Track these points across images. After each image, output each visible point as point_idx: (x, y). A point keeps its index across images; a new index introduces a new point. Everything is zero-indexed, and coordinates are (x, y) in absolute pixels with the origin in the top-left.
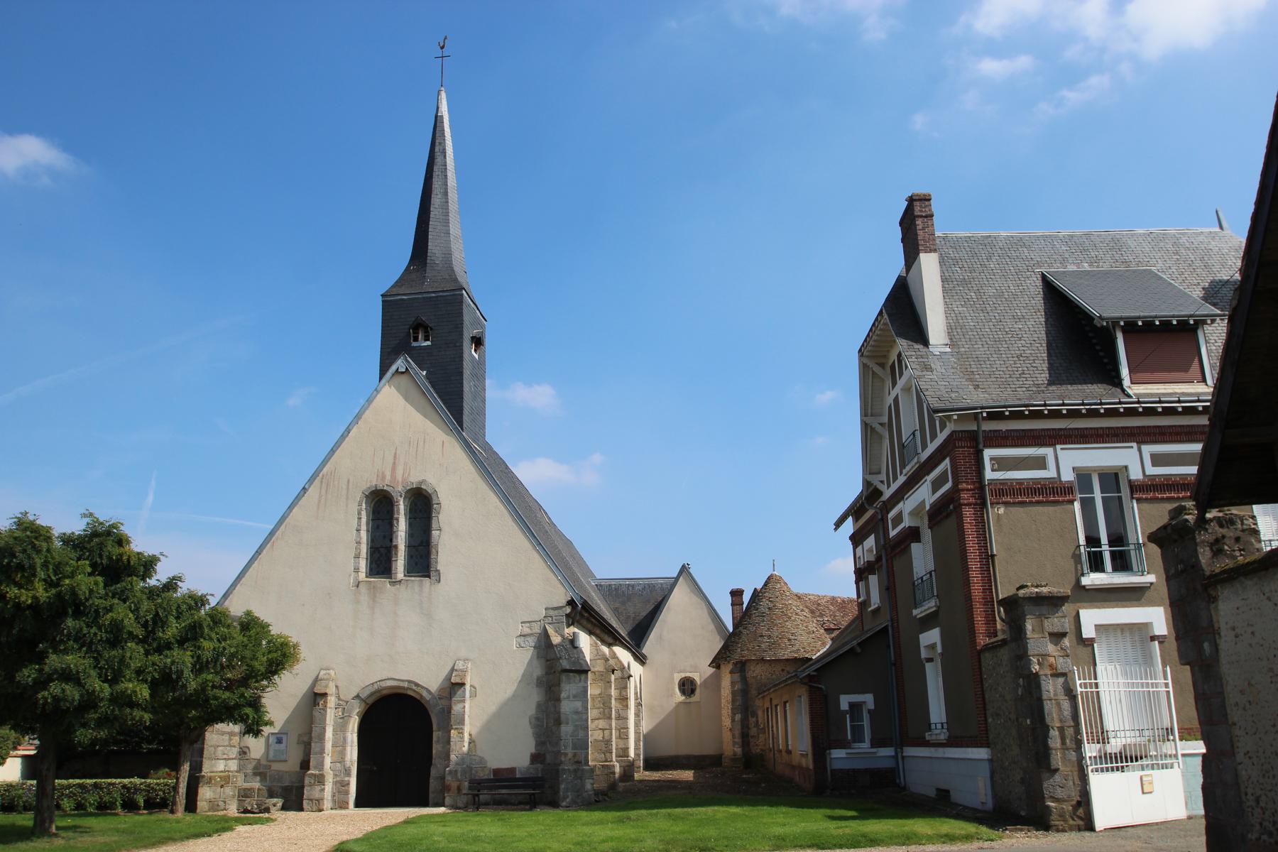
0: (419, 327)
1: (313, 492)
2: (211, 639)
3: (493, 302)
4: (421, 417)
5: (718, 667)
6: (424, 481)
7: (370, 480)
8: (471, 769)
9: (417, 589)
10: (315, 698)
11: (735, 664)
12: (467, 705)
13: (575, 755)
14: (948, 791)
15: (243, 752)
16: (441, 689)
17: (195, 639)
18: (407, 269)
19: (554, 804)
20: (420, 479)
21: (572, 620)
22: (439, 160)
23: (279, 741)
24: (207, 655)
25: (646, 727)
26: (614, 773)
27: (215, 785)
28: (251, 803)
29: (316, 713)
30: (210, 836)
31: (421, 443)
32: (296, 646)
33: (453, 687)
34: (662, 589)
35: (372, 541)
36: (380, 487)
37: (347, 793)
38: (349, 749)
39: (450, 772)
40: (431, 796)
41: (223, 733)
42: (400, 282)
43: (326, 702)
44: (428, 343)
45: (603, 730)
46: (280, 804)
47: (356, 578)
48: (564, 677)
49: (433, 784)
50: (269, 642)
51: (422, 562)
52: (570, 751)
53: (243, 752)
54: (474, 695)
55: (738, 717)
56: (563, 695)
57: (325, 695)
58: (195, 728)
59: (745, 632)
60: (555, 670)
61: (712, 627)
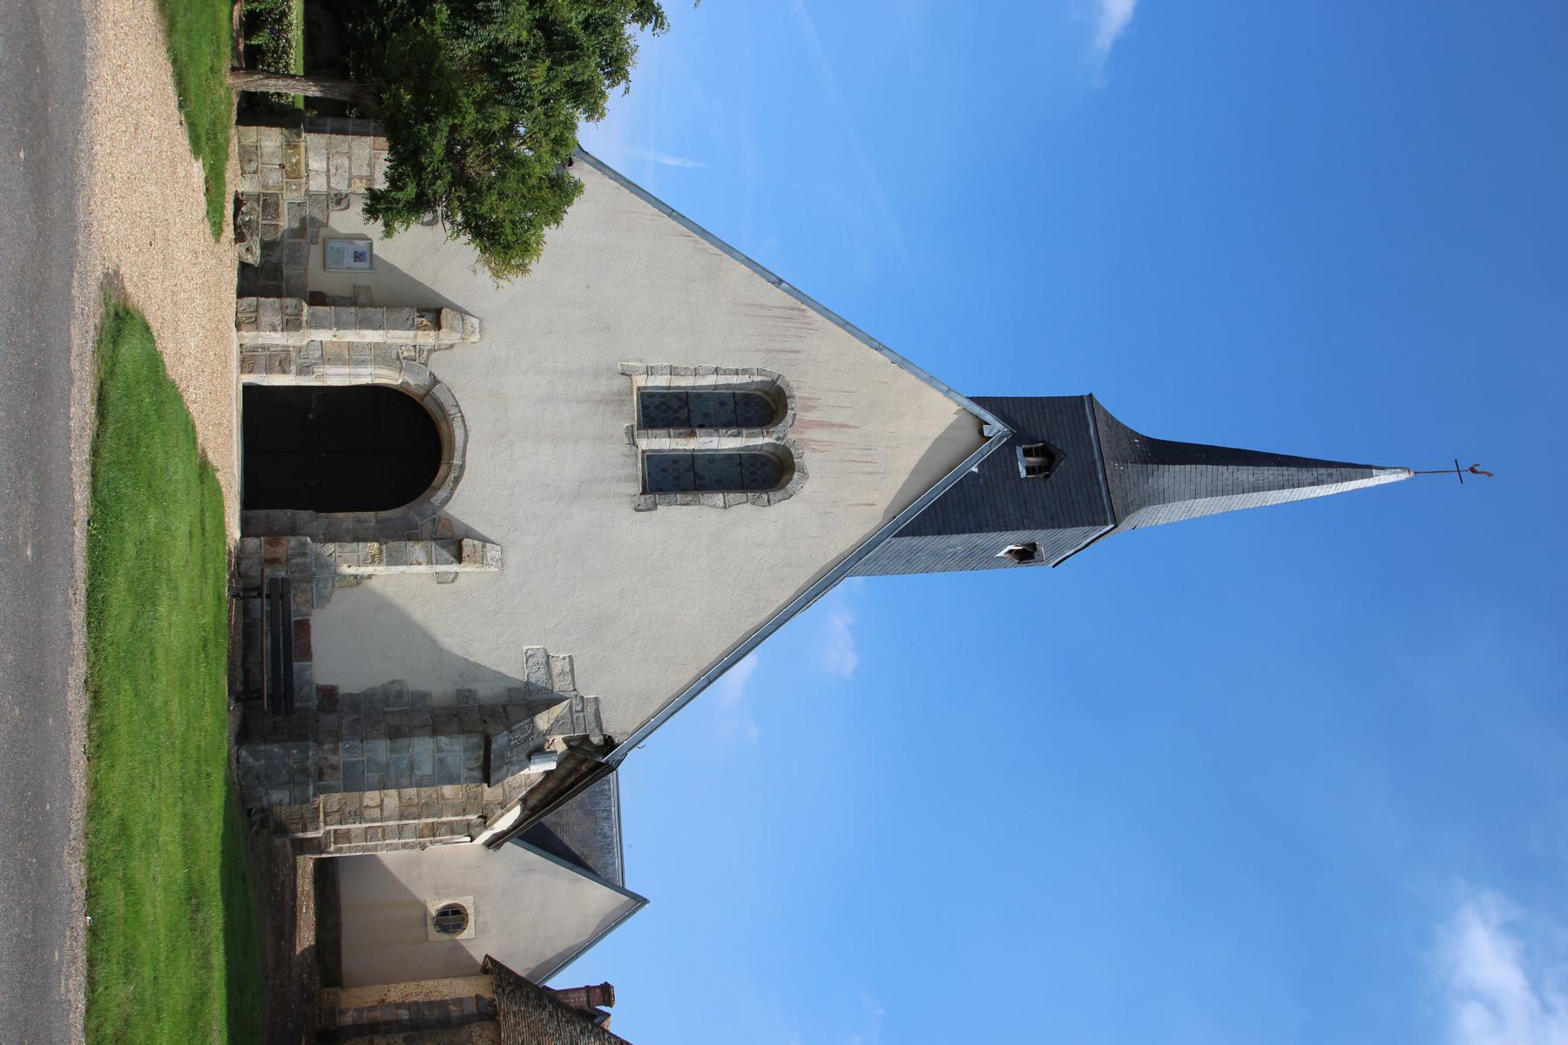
0: (1048, 458)
1: (777, 295)
2: (549, 81)
3: (1087, 573)
4: (912, 466)
5: (485, 970)
6: (805, 475)
7: (801, 386)
8: (309, 581)
9: (623, 473)
10: (432, 312)
11: (491, 1003)
12: (423, 568)
13: (334, 768)
15: (340, 200)
16: (450, 522)
17: (550, 50)
18: (1136, 435)
19: (244, 734)
20: (809, 470)
21: (578, 746)
22: (1306, 474)
23: (358, 257)
24: (519, 70)
25: (381, 854)
26: (305, 830)
27: (285, 156)
28: (252, 212)
29: (406, 313)
30: (181, 106)
31: (868, 468)
32: (522, 268)
33: (454, 543)
34: (606, 865)
35: (699, 396)
36: (791, 404)
37: (269, 370)
38: (345, 370)
39: (304, 544)
40: (262, 513)
41: (371, 166)
42: (1113, 424)
43: (425, 328)
44: (1023, 474)
45: (381, 806)
46: (250, 259)
47: (636, 371)
48: (476, 740)
49: (283, 516)
50: (530, 222)
51: (668, 480)
52: (341, 758)
53: (340, 200)
54: (441, 579)
55: (404, 1014)
56: (443, 740)
57: (438, 326)
58: (380, 101)
59: (545, 1015)
60: (487, 720)
61: (550, 954)
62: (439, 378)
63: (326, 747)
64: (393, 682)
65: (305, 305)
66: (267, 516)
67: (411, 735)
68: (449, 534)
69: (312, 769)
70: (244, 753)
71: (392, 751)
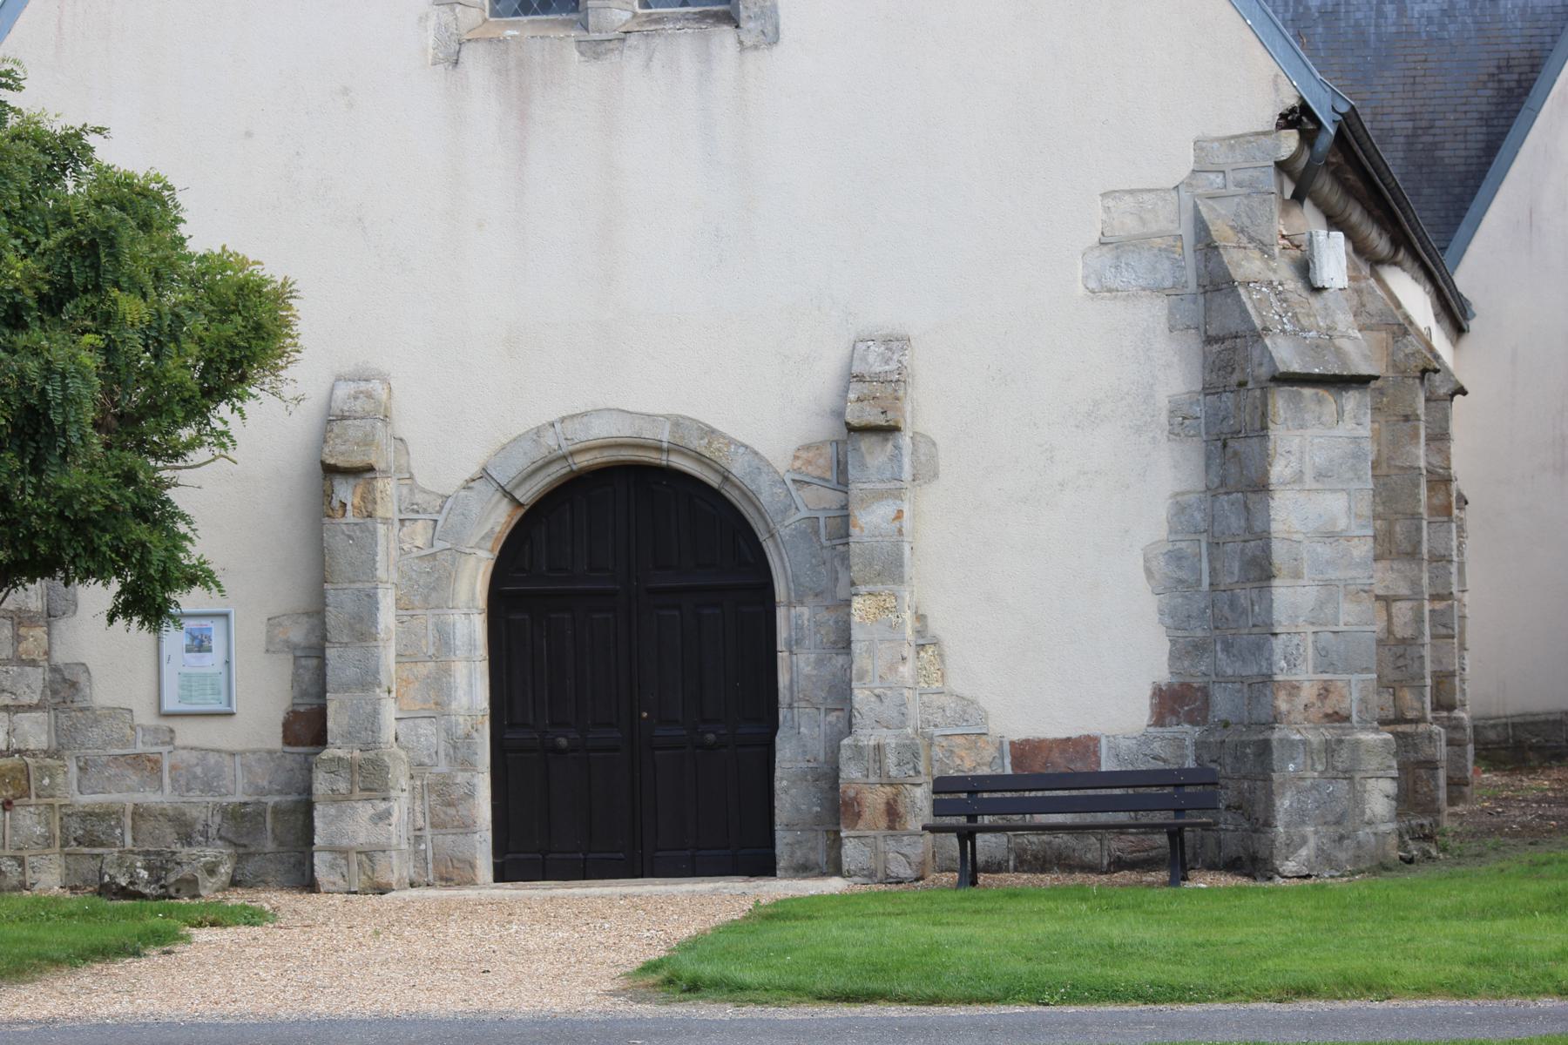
13: (1325, 692)
14: (936, 476)
30: (137, 954)
38: (460, 670)
40: (782, 838)
43: (369, 499)
45: (1387, 600)
48: (1280, 401)
52: (1307, 677)
56: (1279, 471)
62: (474, 470)
63: (1283, 705)
64: (1149, 572)
65: (328, 753)
66: (789, 827)
67: (1265, 537)
68: (829, 451)
69: (1329, 734)
70: (1290, 866)
71: (1297, 575)
